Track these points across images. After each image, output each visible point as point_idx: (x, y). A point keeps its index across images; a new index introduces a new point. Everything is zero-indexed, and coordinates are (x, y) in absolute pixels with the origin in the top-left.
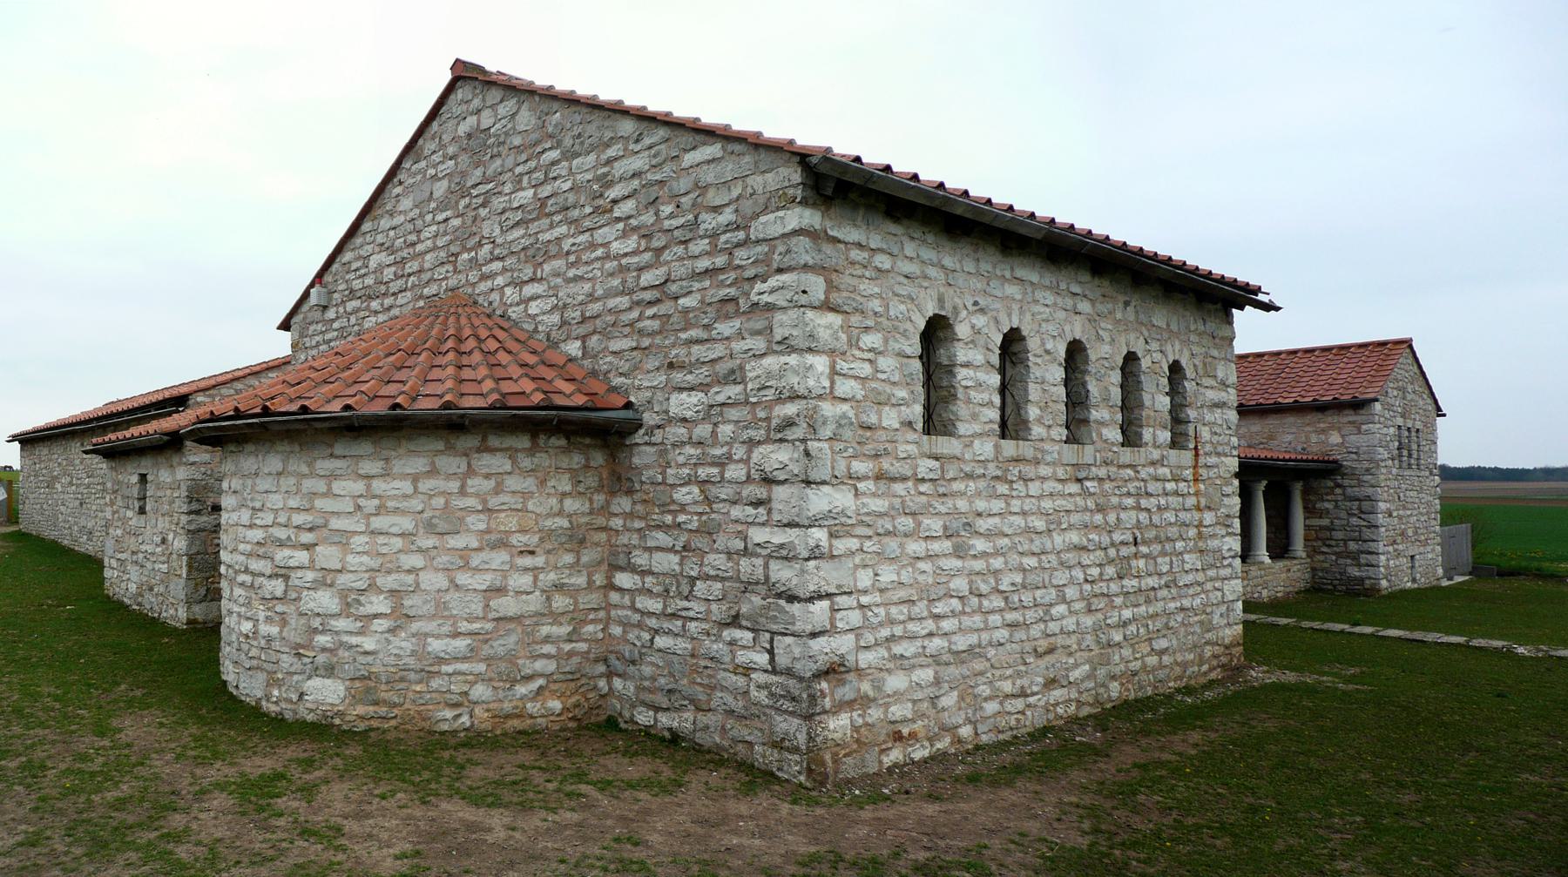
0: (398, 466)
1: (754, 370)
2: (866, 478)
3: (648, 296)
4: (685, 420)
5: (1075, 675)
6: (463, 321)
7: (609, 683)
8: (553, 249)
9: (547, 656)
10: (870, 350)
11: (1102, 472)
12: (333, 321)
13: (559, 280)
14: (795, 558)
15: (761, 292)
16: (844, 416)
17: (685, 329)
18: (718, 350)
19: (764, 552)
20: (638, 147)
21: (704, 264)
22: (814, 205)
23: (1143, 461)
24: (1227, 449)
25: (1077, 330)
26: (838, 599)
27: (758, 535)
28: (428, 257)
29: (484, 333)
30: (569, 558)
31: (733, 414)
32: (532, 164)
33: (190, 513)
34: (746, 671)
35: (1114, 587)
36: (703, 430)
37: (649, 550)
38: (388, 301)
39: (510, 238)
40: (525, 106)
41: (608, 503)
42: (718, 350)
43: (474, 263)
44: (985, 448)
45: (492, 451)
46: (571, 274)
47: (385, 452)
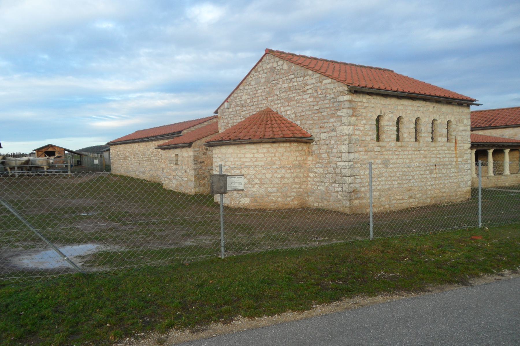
0: (260, 151)
1: (338, 129)
2: (362, 151)
3: (315, 112)
4: (324, 139)
5: (418, 196)
6: (271, 115)
7: (308, 198)
8: (293, 99)
9: (294, 192)
10: (363, 124)
11: (425, 149)
12: (232, 112)
13: (294, 106)
14: (346, 168)
15: (339, 113)
16: (357, 138)
17: (324, 120)
18: (331, 125)
19: (340, 167)
20: (313, 77)
21: (327, 106)
22: (350, 95)
23: (438, 146)
24: (467, 142)
25: (418, 115)
26: (356, 176)
27: (339, 164)
28: (260, 98)
29: (277, 119)
30: (299, 170)
31: (334, 138)
32: (287, 78)
33: (194, 164)
34: (337, 192)
35: (428, 176)
36: (328, 142)
37: (316, 168)
38: (249, 108)
39: (282, 95)
40: (285, 63)
41: (307, 158)
42: (331, 125)
43: (273, 101)
44: (393, 144)
45: (281, 147)
46: (297, 105)
47: (258, 148)
